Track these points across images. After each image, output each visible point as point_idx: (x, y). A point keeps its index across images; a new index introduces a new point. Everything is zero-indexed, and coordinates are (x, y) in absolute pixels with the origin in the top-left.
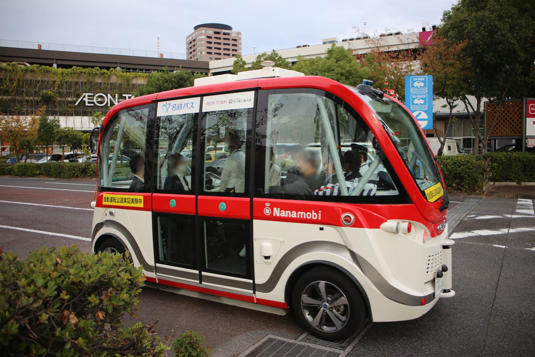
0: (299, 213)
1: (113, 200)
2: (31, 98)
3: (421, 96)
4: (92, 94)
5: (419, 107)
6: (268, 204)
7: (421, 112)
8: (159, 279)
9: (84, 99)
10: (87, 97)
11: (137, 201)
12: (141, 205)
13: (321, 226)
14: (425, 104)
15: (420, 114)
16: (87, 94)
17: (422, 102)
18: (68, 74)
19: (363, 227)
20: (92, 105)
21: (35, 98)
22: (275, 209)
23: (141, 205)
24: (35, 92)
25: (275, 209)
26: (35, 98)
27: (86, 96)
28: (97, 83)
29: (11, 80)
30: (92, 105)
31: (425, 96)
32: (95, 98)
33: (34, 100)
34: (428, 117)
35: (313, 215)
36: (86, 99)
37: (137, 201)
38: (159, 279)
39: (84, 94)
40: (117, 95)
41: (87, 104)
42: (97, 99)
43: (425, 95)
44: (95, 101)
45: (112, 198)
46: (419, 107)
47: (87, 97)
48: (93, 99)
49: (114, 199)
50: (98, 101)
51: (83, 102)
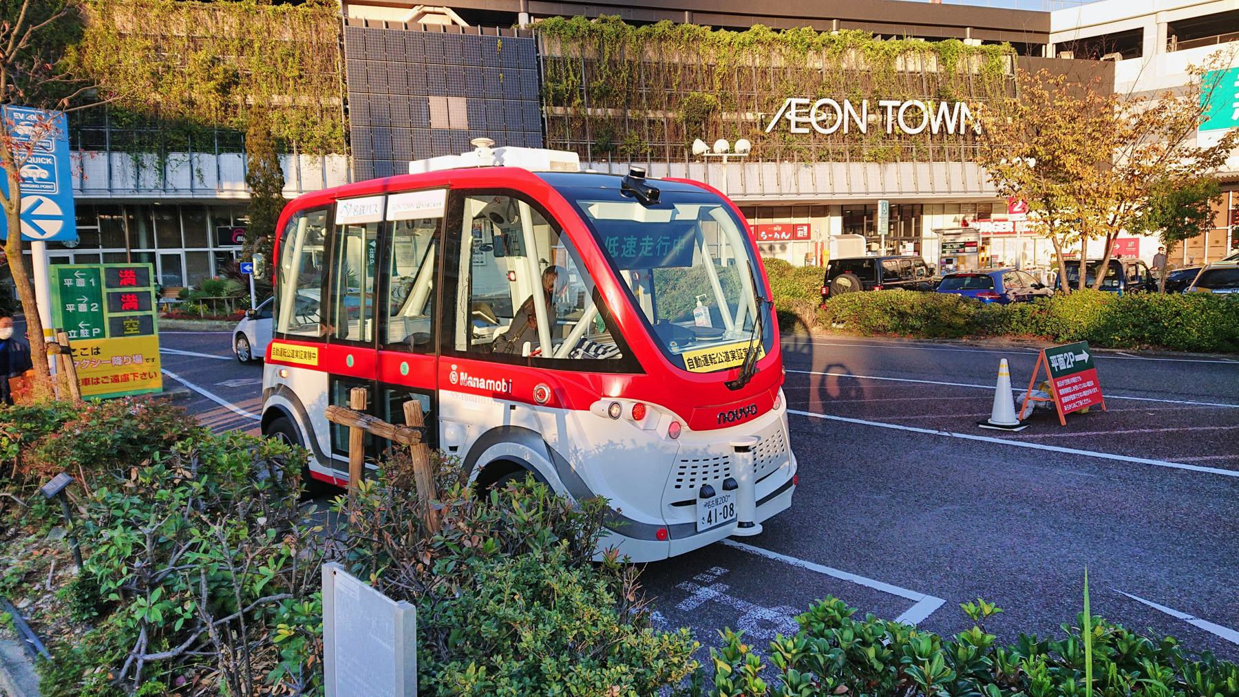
0: (488, 381)
1: (283, 353)
2: (659, 114)
3: (40, 160)
4: (806, 101)
5: (36, 186)
6: (454, 367)
7: (41, 198)
8: (337, 479)
9: (787, 115)
10: (793, 110)
11: (310, 355)
12: (315, 362)
13: (513, 403)
14: (51, 179)
15: (40, 202)
16: (794, 101)
17: (44, 174)
18: (744, 45)
19: (560, 407)
20: (806, 131)
21: (670, 115)
22: (462, 374)
23: (315, 362)
24: (670, 96)
25: (462, 374)
26: (670, 115)
27: (793, 106)
28: (811, 71)
29: (613, 63)
30: (806, 131)
31: (49, 161)
32: (814, 111)
33: (668, 119)
34: (61, 206)
35: (501, 386)
36: (791, 116)
37: (310, 355)
38: (337, 479)
39: (788, 100)
40: (865, 102)
41: (793, 129)
42: (817, 115)
43: (49, 157)
44: (813, 120)
45: (705, 357)
46: (36, 186)
47: (793, 110)
48: (808, 114)
49: (711, 359)
50: (820, 119)
51: (783, 125)
